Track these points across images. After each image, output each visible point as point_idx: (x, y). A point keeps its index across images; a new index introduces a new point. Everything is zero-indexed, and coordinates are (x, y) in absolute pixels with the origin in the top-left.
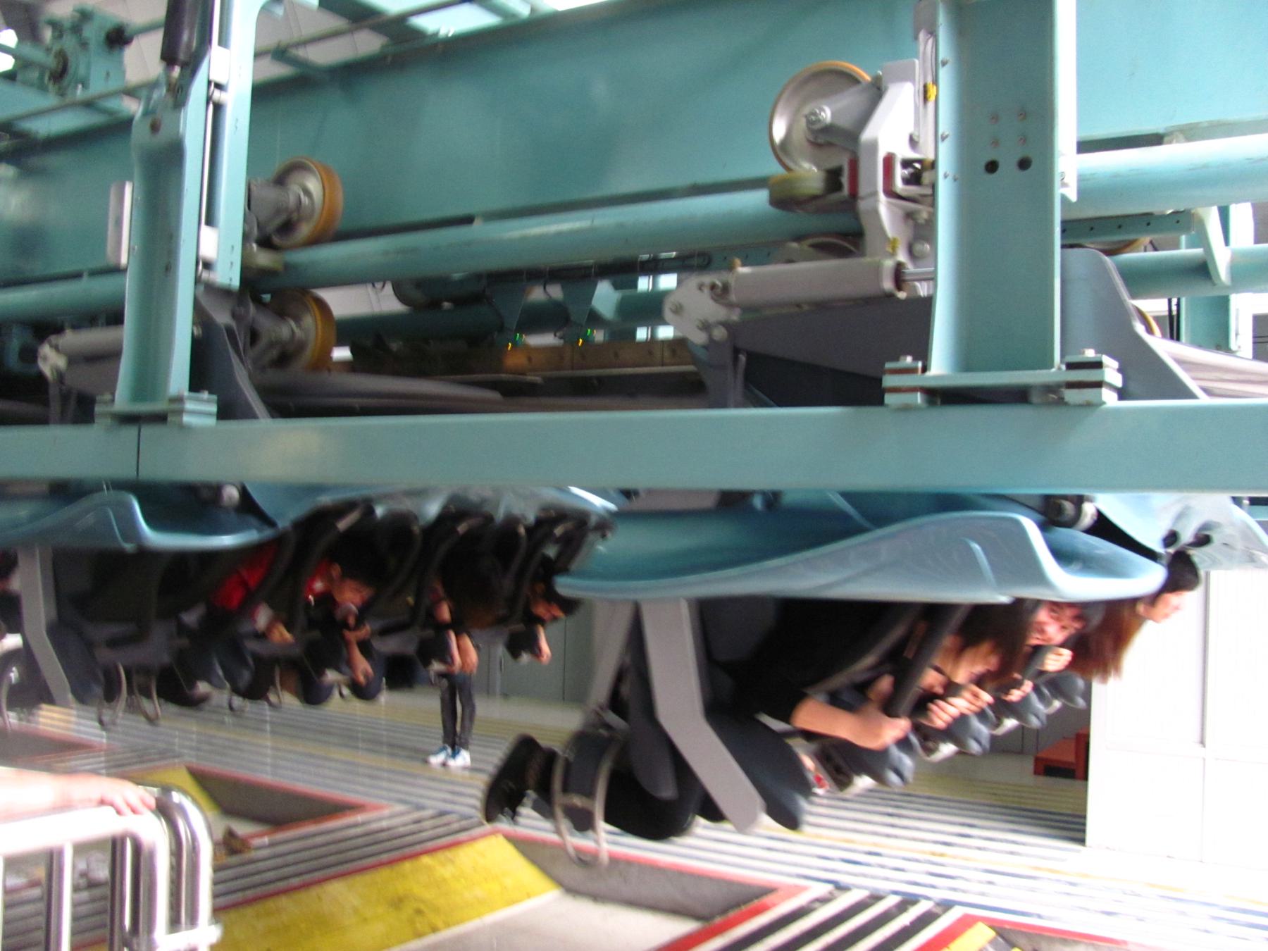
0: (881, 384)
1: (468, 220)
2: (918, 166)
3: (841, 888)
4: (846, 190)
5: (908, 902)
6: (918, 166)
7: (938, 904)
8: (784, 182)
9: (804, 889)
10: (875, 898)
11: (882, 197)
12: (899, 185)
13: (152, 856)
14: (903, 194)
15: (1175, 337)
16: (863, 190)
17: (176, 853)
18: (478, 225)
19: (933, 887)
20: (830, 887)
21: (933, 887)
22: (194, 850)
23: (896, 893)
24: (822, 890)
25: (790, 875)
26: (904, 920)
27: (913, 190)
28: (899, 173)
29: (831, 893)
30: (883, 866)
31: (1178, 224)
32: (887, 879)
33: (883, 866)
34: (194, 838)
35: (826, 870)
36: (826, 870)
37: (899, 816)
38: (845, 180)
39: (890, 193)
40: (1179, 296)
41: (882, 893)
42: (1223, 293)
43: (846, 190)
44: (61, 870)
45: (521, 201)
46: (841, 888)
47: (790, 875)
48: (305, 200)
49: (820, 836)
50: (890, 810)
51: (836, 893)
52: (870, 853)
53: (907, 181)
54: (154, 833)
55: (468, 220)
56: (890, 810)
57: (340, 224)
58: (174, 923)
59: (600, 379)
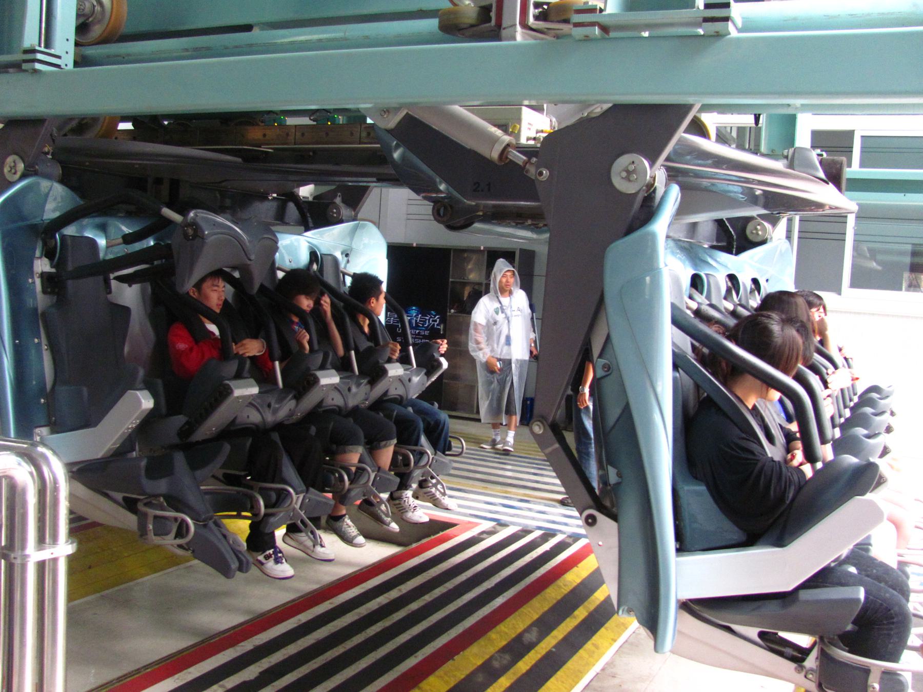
0: (517, 164)
1: (248, 28)
2: (545, 7)
3: (503, 525)
4: (493, 22)
5: (548, 535)
6: (545, 7)
7: (569, 536)
8: (448, 13)
9: (477, 524)
10: (526, 532)
11: (518, 28)
12: (531, 20)
13: (24, 492)
14: (534, 27)
15: (850, 149)
16: (505, 23)
17: (42, 493)
18: (256, 31)
19: (566, 524)
20: (493, 524)
21: (566, 524)
22: (56, 489)
23: (540, 528)
24: (487, 525)
25: (465, 515)
26: (546, 547)
27: (541, 25)
28: (532, 11)
29: (494, 527)
30: (530, 510)
31: (68, 38)
32: (533, 519)
33: (530, 510)
34: (55, 482)
35: (491, 512)
36: (491, 512)
37: (542, 475)
38: (493, 14)
39: (525, 25)
40: (758, 112)
41: (530, 529)
42: (793, 112)
43: (493, 22)
44: (24, 516)
45: (290, 16)
46: (503, 525)
47: (465, 515)
48: (98, 8)
49: (509, 492)
50: (533, 471)
51: (498, 528)
52: (521, 501)
53: (537, 18)
54: (22, 473)
55: (248, 28)
56: (533, 471)
57: (125, 29)
58: (41, 541)
59: (315, 151)
